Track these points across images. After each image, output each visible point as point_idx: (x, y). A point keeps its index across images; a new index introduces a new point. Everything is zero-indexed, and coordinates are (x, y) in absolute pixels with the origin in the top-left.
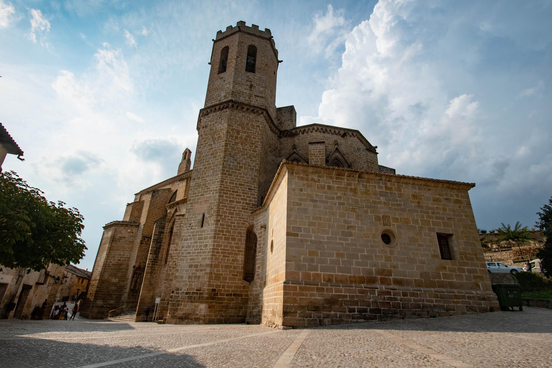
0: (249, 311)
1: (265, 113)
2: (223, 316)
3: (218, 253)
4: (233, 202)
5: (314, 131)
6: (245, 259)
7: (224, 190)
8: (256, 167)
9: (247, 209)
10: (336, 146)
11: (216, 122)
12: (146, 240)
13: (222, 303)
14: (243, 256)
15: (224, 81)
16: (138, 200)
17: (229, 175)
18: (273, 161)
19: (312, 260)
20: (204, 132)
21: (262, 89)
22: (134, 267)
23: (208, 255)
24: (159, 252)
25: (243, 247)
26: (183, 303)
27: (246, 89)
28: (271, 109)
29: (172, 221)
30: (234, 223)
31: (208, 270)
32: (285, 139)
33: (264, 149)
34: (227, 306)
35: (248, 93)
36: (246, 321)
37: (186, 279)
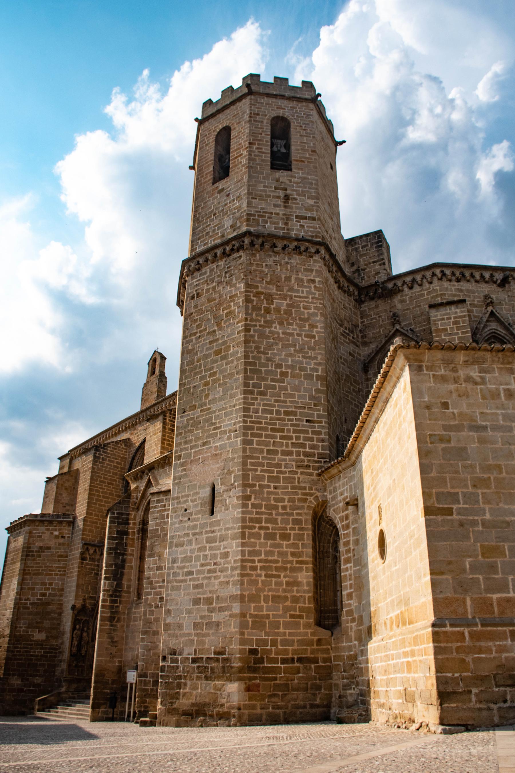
0: (336, 694)
1: (323, 251)
2: (279, 707)
3: (254, 568)
4: (276, 452)
5: (435, 280)
6: (315, 578)
7: (252, 428)
8: (317, 370)
9: (308, 467)
10: (490, 309)
11: (219, 283)
12: (91, 551)
13: (275, 679)
14: (311, 574)
15: (228, 195)
16: (66, 470)
17: (261, 393)
18: (350, 354)
19: (492, 568)
20: (196, 307)
21: (311, 202)
22: (73, 607)
23: (233, 576)
24: (122, 574)
25: (307, 553)
26: (189, 683)
27: (275, 206)
28: (334, 242)
29: (142, 508)
30: (283, 500)
31: (236, 608)
32: (373, 304)
33: (329, 330)
34: (287, 685)
35: (281, 213)
36: (332, 716)
37: (188, 629)
